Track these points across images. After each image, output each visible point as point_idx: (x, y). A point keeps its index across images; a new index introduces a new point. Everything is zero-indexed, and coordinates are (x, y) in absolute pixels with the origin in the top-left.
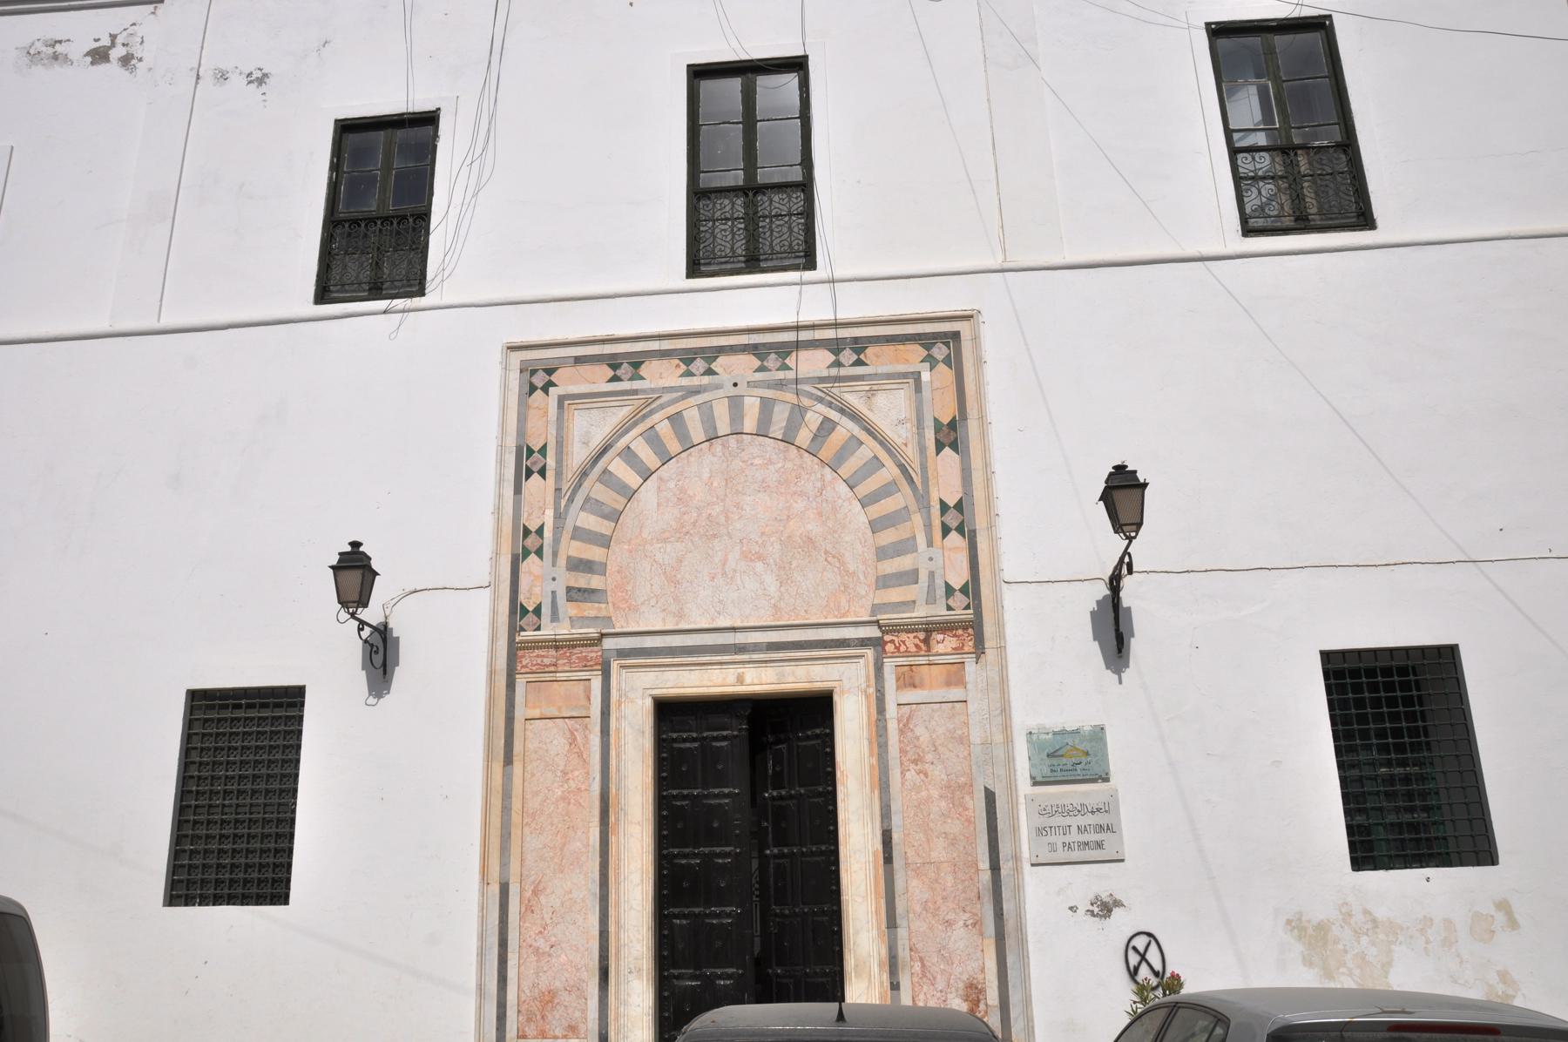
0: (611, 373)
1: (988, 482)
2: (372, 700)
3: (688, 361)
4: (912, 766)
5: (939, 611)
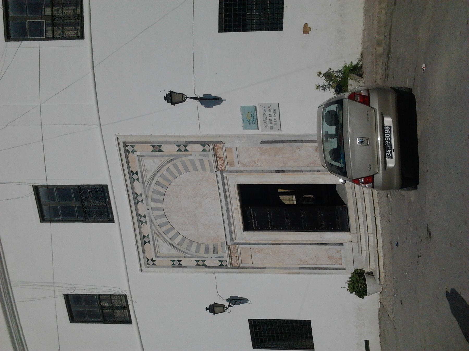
0: (147, 244)
1: (171, 136)
2: (249, 302)
3: (142, 222)
5: (211, 154)
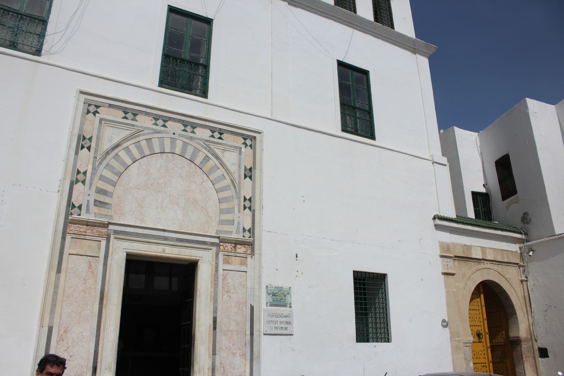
3: (156, 119)
4: (226, 293)
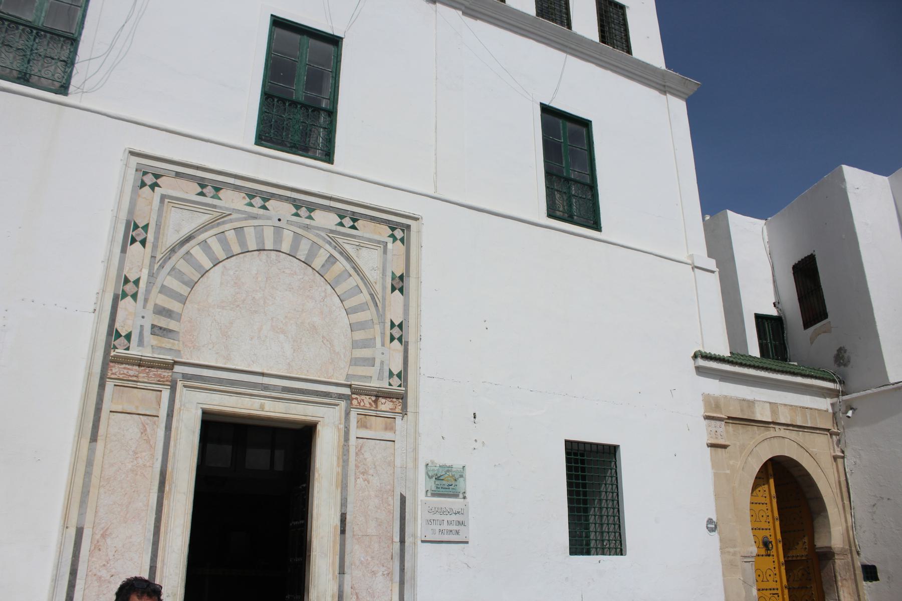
3: (251, 197)
5: (383, 384)
